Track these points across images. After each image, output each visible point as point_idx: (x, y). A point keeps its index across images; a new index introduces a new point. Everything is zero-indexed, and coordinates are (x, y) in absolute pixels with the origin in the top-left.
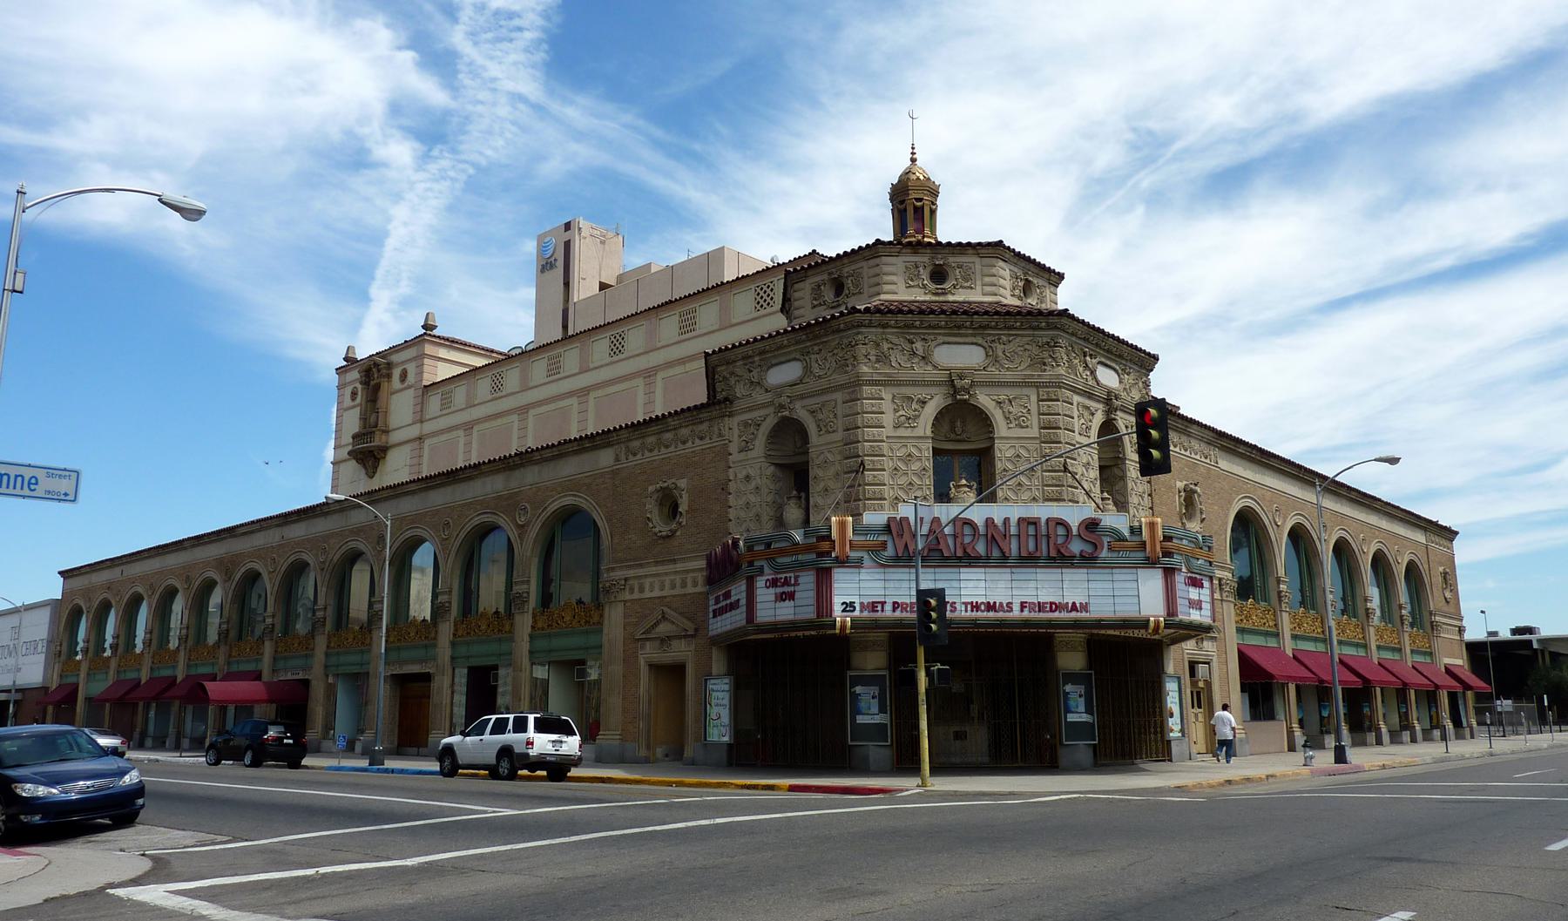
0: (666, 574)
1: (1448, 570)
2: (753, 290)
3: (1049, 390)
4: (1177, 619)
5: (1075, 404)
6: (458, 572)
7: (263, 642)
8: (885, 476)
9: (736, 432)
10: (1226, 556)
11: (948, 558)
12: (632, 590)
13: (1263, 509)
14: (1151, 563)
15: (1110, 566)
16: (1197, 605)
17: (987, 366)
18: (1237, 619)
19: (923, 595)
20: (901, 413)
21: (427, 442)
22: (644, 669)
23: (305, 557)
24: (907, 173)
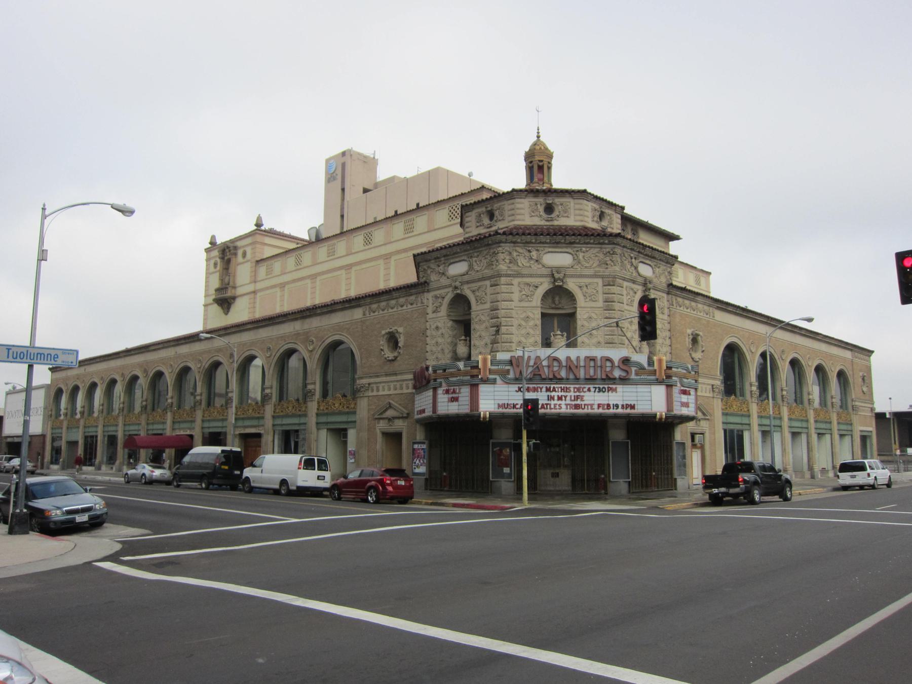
0: (391, 382)
1: (865, 374)
2: (447, 208)
3: (610, 281)
4: (673, 413)
5: (625, 287)
6: (276, 376)
7: (166, 413)
8: (513, 330)
9: (431, 301)
10: (717, 371)
11: (544, 379)
12: (372, 391)
13: (743, 343)
14: (659, 382)
15: (636, 383)
16: (686, 405)
17: (574, 265)
18: (724, 407)
19: (526, 402)
20: (524, 293)
21: (259, 295)
22: (379, 436)
23: (189, 364)
24: (535, 144)
